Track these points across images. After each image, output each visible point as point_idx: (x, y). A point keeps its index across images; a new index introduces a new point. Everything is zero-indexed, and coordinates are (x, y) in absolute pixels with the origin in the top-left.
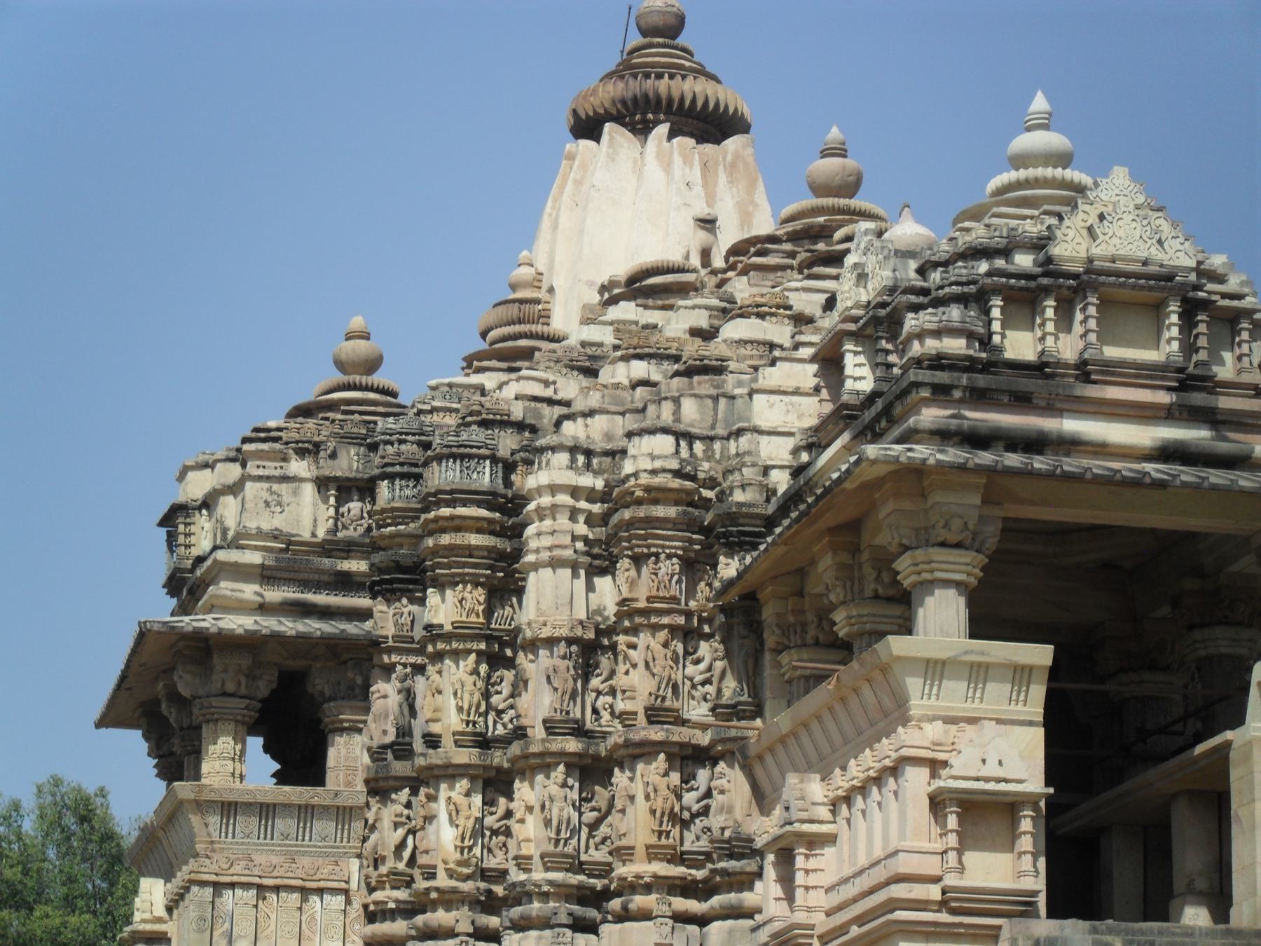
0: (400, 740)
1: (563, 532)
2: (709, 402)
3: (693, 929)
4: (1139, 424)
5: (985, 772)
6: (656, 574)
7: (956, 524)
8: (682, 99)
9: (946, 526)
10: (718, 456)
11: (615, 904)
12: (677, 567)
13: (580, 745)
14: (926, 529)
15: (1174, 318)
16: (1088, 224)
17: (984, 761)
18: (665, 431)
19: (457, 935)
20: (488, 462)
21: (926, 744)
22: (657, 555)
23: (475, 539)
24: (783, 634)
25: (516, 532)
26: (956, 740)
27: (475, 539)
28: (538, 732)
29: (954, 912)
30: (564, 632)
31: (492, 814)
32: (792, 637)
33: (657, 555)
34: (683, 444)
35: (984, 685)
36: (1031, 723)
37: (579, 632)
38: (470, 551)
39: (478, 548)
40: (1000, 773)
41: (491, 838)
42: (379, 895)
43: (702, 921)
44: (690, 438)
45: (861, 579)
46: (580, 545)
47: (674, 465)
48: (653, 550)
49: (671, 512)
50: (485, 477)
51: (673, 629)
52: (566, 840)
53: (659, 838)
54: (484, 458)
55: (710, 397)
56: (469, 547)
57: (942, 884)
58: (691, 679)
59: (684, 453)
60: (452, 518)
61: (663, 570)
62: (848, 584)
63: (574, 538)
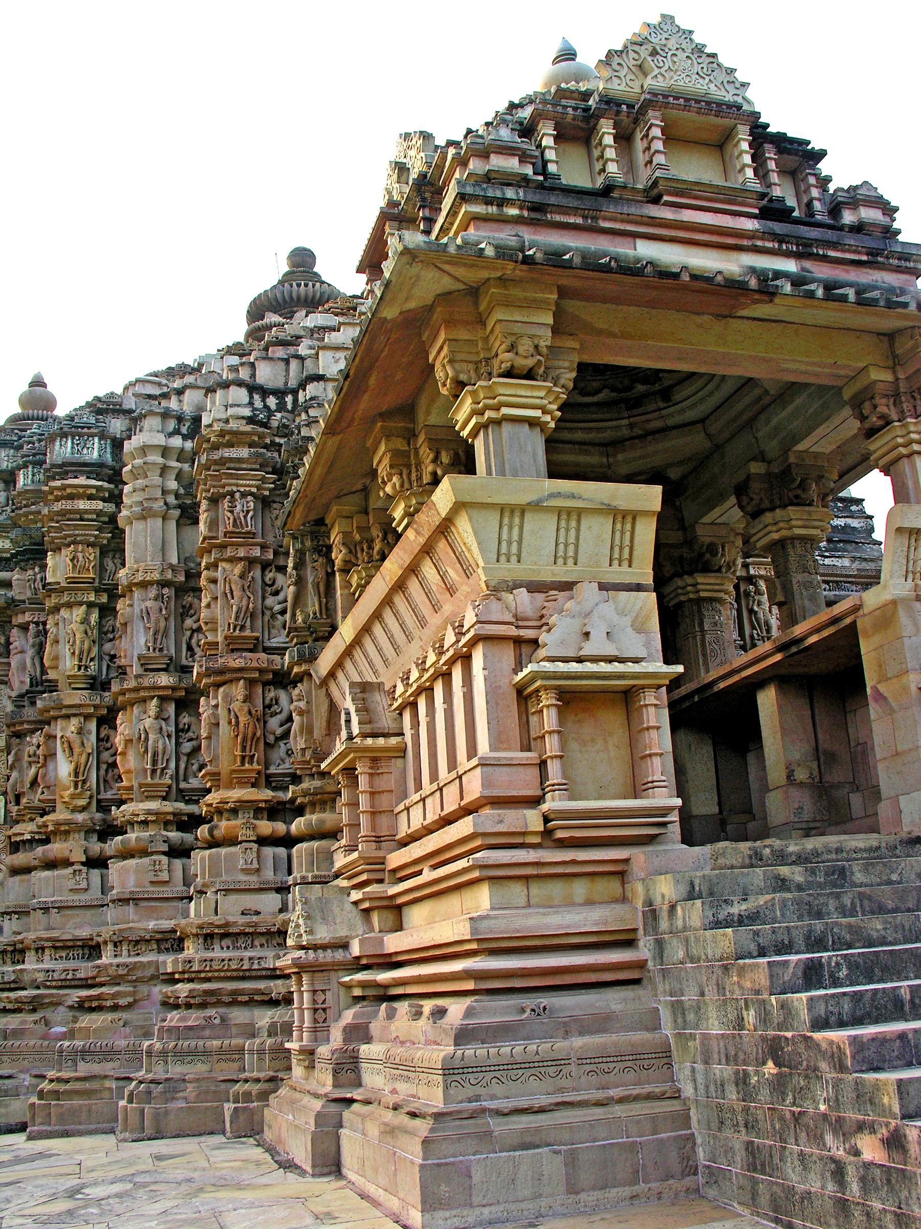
0: (34, 689)
1: (154, 486)
2: (282, 365)
3: (282, 851)
4: (720, 251)
5: (588, 649)
6: (232, 512)
7: (525, 346)
8: (314, 296)
9: (512, 348)
10: (289, 407)
11: (203, 831)
12: (252, 504)
13: (171, 679)
14: (487, 360)
15: (745, 146)
16: (639, 63)
17: (587, 634)
18: (240, 384)
19: (73, 864)
20: (96, 439)
21: (508, 618)
22: (232, 494)
23: (82, 505)
24: (350, 552)
25: (116, 499)
26: (544, 612)
28: (136, 669)
29: (563, 844)
30: (156, 576)
31: (107, 749)
32: (359, 555)
33: (232, 494)
34: (256, 397)
35: (579, 522)
36: (638, 588)
37: (169, 575)
38: (82, 515)
39: (86, 511)
40: (610, 650)
41: (107, 771)
42: (17, 829)
43: (288, 841)
44: (265, 392)
45: (418, 465)
46: (171, 499)
47: (247, 412)
48: (227, 488)
49: (244, 452)
50: (94, 451)
51: (251, 562)
52: (163, 769)
53: (243, 764)
54: (93, 436)
55: (282, 359)
56: (78, 511)
57: (545, 807)
58: (271, 609)
59: (258, 404)
60: (64, 487)
61: (239, 508)
62: (405, 472)
63: (164, 492)
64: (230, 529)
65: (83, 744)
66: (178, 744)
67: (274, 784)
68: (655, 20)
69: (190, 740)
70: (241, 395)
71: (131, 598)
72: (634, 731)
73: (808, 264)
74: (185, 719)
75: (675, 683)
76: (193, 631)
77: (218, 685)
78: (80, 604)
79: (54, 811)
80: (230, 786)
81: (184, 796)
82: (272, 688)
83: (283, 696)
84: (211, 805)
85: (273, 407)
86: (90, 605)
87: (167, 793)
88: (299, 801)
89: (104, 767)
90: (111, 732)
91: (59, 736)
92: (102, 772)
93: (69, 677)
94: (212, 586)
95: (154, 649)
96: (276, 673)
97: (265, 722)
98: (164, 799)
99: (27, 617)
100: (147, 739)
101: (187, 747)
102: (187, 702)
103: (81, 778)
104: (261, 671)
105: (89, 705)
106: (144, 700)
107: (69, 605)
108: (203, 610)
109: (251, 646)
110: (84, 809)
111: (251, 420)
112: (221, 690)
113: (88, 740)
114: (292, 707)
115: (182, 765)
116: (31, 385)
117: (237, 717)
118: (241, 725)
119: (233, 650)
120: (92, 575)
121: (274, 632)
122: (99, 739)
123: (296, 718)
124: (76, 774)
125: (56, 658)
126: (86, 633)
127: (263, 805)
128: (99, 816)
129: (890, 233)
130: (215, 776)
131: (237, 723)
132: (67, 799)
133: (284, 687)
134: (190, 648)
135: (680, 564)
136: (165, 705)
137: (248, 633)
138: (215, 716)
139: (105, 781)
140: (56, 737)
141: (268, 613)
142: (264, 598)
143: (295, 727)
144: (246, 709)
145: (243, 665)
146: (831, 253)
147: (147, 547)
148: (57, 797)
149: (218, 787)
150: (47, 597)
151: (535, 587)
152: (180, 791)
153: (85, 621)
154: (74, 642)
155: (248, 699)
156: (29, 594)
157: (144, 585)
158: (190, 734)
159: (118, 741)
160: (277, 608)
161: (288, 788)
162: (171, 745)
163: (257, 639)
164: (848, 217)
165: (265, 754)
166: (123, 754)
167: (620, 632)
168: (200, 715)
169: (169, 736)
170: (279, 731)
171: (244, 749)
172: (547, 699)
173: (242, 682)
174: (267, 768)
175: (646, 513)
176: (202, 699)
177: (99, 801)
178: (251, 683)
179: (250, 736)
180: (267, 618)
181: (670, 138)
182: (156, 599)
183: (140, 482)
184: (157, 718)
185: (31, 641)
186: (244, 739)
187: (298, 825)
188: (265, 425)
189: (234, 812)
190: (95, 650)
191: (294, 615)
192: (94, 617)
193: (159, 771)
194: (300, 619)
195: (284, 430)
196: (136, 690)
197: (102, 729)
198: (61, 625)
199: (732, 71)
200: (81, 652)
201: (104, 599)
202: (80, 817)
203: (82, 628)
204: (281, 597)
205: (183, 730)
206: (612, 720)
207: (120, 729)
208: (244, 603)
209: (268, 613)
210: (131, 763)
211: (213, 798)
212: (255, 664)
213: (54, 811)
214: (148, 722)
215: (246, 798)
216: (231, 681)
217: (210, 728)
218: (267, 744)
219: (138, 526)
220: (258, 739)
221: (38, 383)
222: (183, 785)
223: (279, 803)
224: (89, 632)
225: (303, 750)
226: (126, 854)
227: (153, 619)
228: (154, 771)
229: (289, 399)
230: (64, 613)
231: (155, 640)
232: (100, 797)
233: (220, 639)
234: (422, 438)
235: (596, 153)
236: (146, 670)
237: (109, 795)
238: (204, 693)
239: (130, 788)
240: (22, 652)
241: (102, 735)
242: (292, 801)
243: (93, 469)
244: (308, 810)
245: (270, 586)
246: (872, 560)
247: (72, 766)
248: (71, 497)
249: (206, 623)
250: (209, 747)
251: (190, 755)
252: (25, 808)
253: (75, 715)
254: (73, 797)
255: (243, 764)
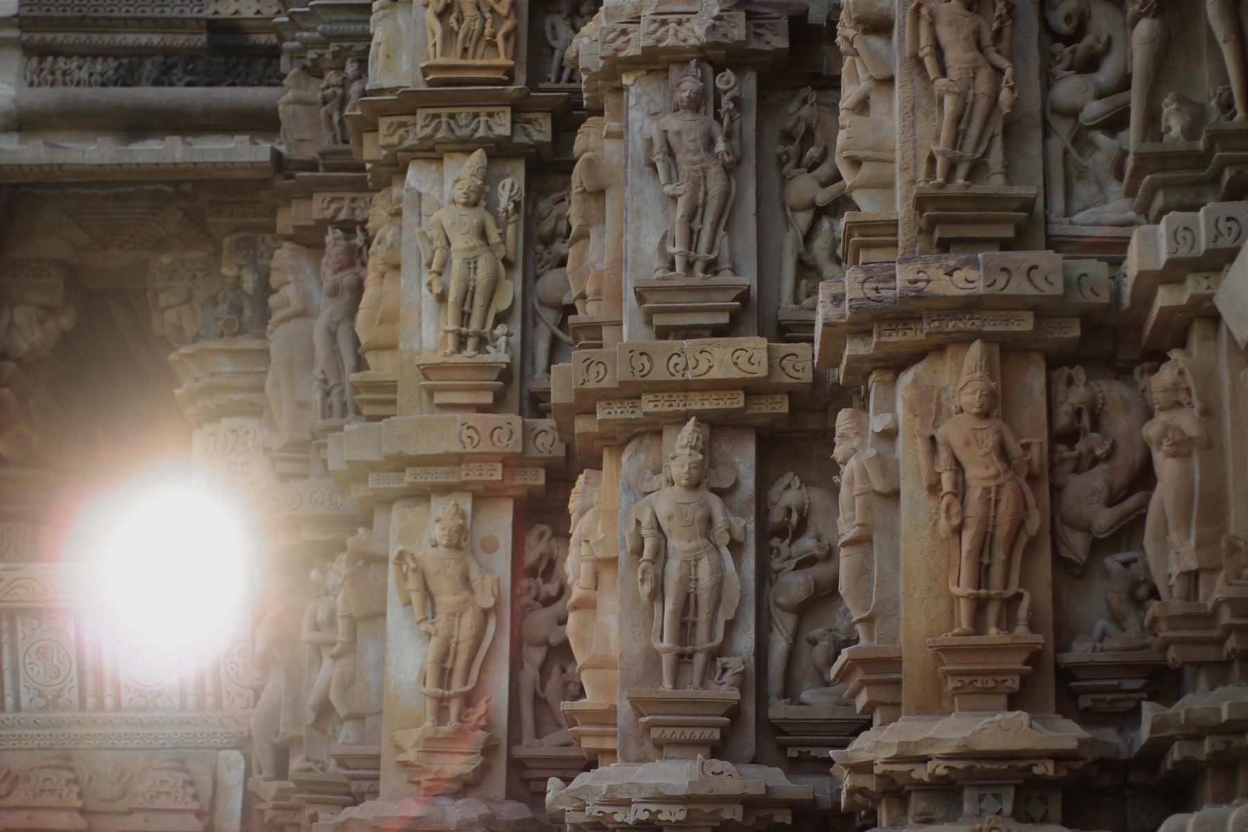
28: (632, 329)
41: (544, 670)
52: (714, 655)
58: (1074, 113)
65: (466, 581)
66: (764, 576)
67: (1085, 702)
69: (806, 563)
71: (621, 113)
74: (789, 494)
76: (820, 213)
77: (896, 364)
78: (466, 146)
79: (375, 794)
80: (932, 706)
81: (783, 748)
82: (1080, 373)
83: (1112, 391)
84: (865, 768)
86: (499, 151)
87: (728, 733)
88: (1176, 753)
89: (536, 656)
91: (393, 555)
92: (530, 673)
93: (427, 370)
94: (876, 42)
95: (689, 266)
96: (1092, 321)
97: (1056, 490)
98: (716, 751)
99: (318, 208)
100: (661, 554)
101: (794, 585)
102: (790, 433)
103: (457, 687)
104: (1043, 310)
105: (485, 458)
106: (653, 429)
107: (432, 152)
108: (844, 118)
109: (1008, 232)
112: (906, 378)
113: (485, 569)
114: (1152, 430)
115: (779, 645)
117: (958, 467)
118: (974, 495)
119: (944, 246)
120: (503, 60)
121: (1083, 190)
123: (1166, 467)
124: (444, 675)
125: (390, 318)
126: (483, 234)
127: (1045, 769)
130: (883, 670)
131: (960, 490)
132: (411, 756)
133: (1123, 373)
136: (724, 447)
137: (994, 184)
138: (886, 466)
139: (539, 701)
140: (384, 560)
141: (1063, 129)
142: (1048, 80)
143: (1164, 495)
144: (990, 440)
145: (980, 288)
148: (385, 750)
149: (894, 709)
152: (771, 729)
153: (480, 198)
154: (446, 264)
155: (996, 406)
156: (326, 142)
157: (655, 62)
158: (807, 543)
159: (575, 566)
160: (1094, 109)
161: (1134, 715)
163: (1027, 205)
165: (1057, 600)
166: (587, 605)
168: (835, 468)
169: (736, 547)
170: (1104, 519)
171: (982, 574)
173: (976, 348)
174: (1062, 646)
176: (843, 420)
177: (516, 765)
178: (1007, 351)
179: (1002, 532)
180: (1058, 144)
182: (695, 105)
184: (694, 485)
185: (329, 278)
186: (985, 544)
190: (510, 290)
191: (1152, 119)
192: (511, 186)
193: (699, 659)
194: (1174, 124)
196: (630, 392)
197: (531, 539)
198: (408, 217)
200: (467, 295)
201: (541, 131)
203: (471, 218)
204: (1107, 73)
205: (781, 532)
207: (577, 529)
208: (983, 85)
209: (1063, 129)
210: (610, 633)
211: (874, 746)
212: (1019, 287)
213: (375, 794)
214: (666, 502)
215: (989, 743)
216: (940, 349)
217: (867, 509)
218: (1061, 563)
220: (1032, 544)
222: (779, 710)
223: (1106, 764)
224: (494, 236)
225: (1192, 577)
227: (685, 168)
228: (683, 659)
230: (417, 176)
231: (692, 238)
232: (521, 751)
233: (901, 209)
236: (663, 333)
237: (549, 746)
238: (851, 394)
239: (605, 717)
240: (303, 314)
241: (531, 557)
242: (1155, 751)
244: (1208, 787)
245: (1069, 40)
247: (432, 649)
249: (856, 163)
250: (863, 572)
251: (805, 610)
252: (302, 785)
253: (446, 490)
254: (431, 746)
255: (978, 625)
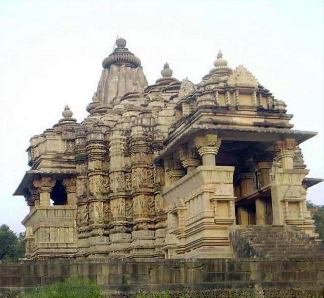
3: (153, 231)
5: (222, 194)
19: (99, 235)
23: (98, 151)
27: (98, 151)
28: (116, 191)
29: (217, 224)
30: (121, 170)
36: (230, 183)
40: (225, 194)
43: (155, 229)
47: (142, 133)
51: (145, 167)
63: (121, 149)
64: (140, 160)
68: (238, 66)
70: (140, 128)
72: (229, 207)
73: (266, 120)
75: (235, 199)
85: (148, 130)
90: (306, 201)
104: (148, 192)
110: (101, 223)
111: (143, 134)
116: (65, 109)
122: (104, 207)
128: (105, 225)
129: (285, 111)
134: (127, 186)
135: (238, 183)
146: (271, 117)
147: (117, 162)
150: (89, 173)
151: (213, 183)
162: (124, 208)
164: (276, 108)
167: (228, 191)
172: (215, 202)
175: (232, 171)
181: (240, 94)
183: (115, 147)
187: (157, 225)
188: (146, 135)
189: (142, 223)
195: (151, 136)
199: (254, 77)
202: (101, 225)
206: (225, 205)
219: (115, 157)
221: (67, 109)
226: (115, 232)
229: (152, 129)
230: (94, 176)
234: (189, 149)
235: (226, 97)
243: (100, 142)
246: (300, 162)
248: (95, 149)
